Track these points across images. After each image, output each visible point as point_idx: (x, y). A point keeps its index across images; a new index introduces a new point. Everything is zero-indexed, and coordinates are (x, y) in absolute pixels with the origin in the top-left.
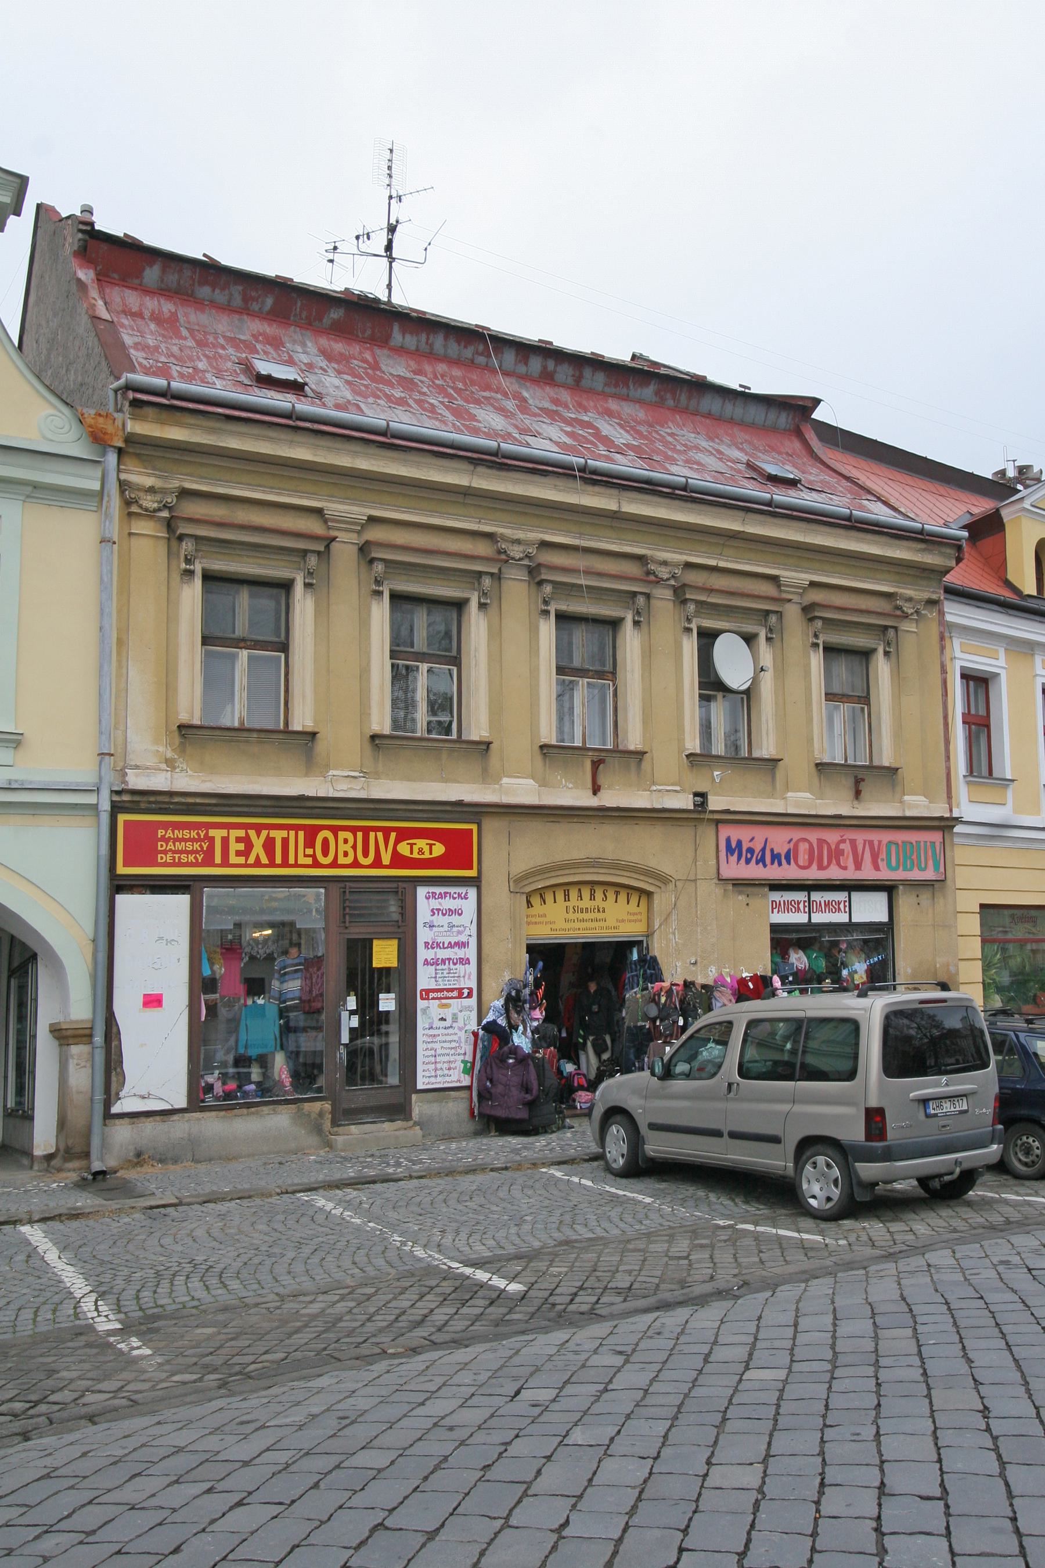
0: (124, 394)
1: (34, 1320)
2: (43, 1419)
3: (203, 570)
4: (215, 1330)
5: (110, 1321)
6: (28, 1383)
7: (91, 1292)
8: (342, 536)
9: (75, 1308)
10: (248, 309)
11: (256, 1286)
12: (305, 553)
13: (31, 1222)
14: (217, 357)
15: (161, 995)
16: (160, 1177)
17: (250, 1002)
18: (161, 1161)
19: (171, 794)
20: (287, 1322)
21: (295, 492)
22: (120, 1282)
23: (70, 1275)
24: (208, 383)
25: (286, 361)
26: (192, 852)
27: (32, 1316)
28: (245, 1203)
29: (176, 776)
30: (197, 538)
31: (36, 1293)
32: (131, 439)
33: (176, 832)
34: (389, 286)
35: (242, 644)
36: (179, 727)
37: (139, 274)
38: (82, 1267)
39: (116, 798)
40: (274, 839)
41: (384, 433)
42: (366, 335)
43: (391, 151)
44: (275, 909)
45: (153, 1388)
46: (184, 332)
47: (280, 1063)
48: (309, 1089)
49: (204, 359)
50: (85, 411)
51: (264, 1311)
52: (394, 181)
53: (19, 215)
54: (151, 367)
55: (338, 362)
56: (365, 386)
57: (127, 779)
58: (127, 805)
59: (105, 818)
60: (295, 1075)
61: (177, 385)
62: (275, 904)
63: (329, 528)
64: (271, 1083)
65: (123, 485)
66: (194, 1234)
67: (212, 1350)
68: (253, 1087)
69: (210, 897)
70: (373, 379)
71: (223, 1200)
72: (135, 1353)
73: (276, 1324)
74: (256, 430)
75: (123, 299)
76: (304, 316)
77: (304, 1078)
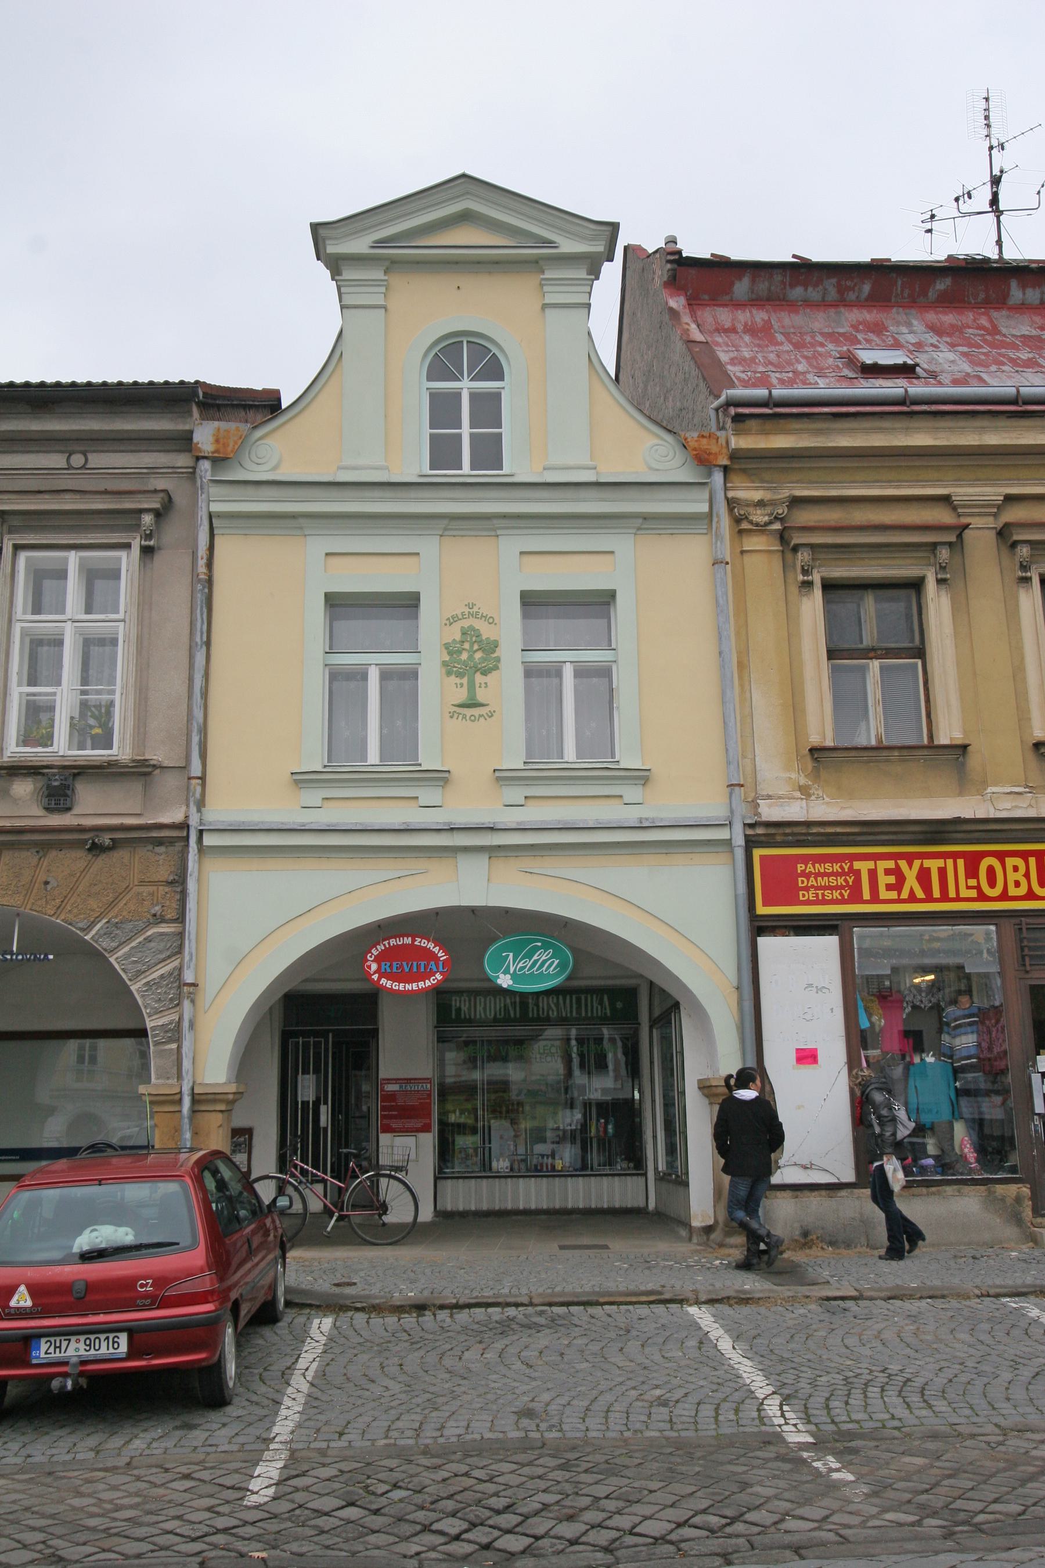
0: (725, 412)
1: (716, 1418)
2: (742, 1540)
3: (823, 579)
4: (927, 1461)
5: (799, 1431)
6: (719, 1494)
7: (774, 1393)
8: (976, 522)
9: (759, 1410)
10: (845, 300)
11: (968, 1412)
12: (934, 546)
13: (698, 1303)
14: (816, 356)
15: (816, 1050)
16: (833, 1262)
17: (917, 1060)
18: (832, 1243)
19: (808, 824)
20: (1016, 1465)
21: (917, 482)
22: (803, 1384)
23: (748, 1369)
24: (810, 384)
25: (892, 345)
26: (836, 888)
27: (713, 1414)
28: (939, 1303)
29: (812, 804)
30: (812, 546)
31: (715, 1387)
32: (736, 456)
33: (817, 865)
34: (999, 243)
35: (872, 654)
36: (811, 750)
37: (728, 289)
38: (760, 1363)
39: (750, 832)
40: (928, 870)
41: (1014, 402)
42: (979, 300)
43: (987, 99)
44: (939, 951)
45: (863, 1525)
46: (780, 337)
47: (961, 1134)
48: (1001, 1168)
49: (803, 361)
50: (687, 435)
51: (983, 1445)
52: (993, 130)
53: (612, 260)
54: (750, 379)
55: (950, 335)
56: (984, 354)
57: (760, 810)
58: (763, 838)
59: (740, 854)
60: (981, 1150)
61: (778, 392)
62: (937, 945)
63: (959, 516)
64: (954, 1159)
65: (731, 503)
66: (882, 1336)
67: (928, 1487)
68: (930, 1161)
69: (861, 938)
70: (992, 345)
71: (911, 1297)
72: (835, 1476)
73: (1002, 1465)
74: (866, 424)
75: (715, 317)
76: (906, 295)
77: (992, 1153)
